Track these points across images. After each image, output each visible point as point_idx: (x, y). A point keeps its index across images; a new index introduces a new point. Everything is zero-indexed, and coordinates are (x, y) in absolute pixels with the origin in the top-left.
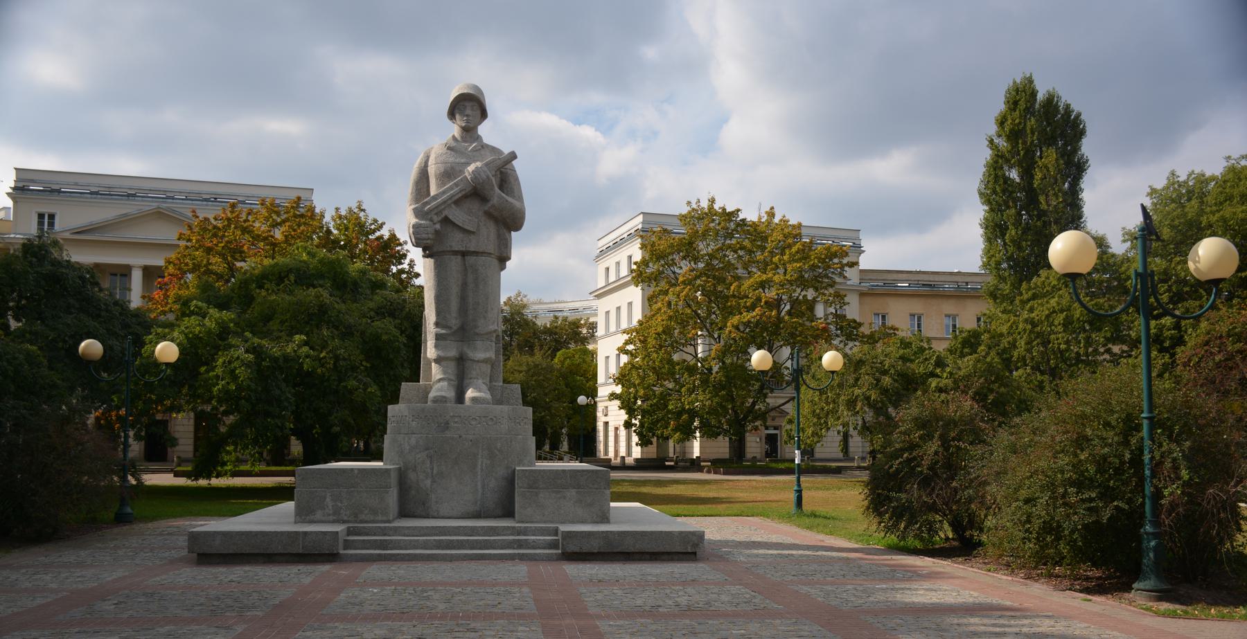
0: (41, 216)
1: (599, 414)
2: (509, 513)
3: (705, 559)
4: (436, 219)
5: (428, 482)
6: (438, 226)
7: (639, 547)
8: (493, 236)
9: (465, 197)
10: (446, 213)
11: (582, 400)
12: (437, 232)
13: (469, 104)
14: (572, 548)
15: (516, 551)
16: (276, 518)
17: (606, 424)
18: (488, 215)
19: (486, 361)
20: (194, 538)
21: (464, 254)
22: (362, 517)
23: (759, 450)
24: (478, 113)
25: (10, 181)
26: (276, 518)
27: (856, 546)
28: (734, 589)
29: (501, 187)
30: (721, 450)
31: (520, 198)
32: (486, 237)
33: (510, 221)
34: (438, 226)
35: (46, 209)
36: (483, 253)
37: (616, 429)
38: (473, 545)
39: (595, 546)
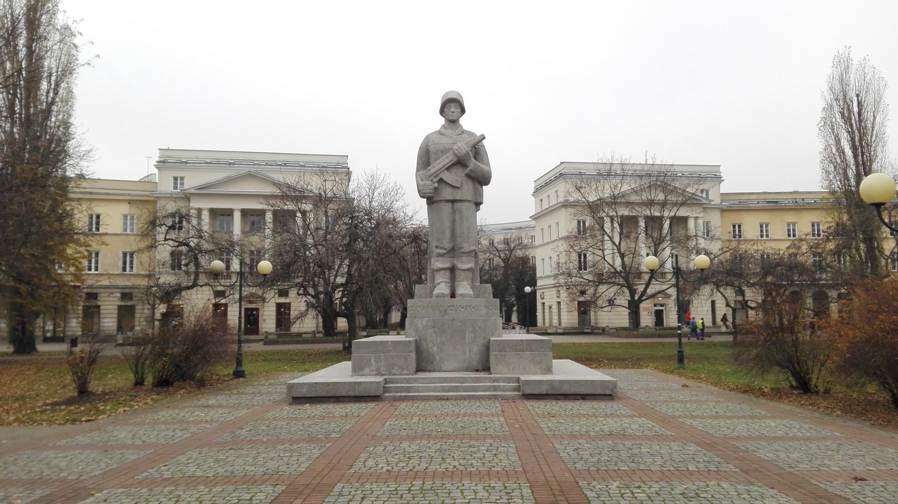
0: (175, 179)
1: (538, 297)
2: (487, 369)
3: (619, 398)
4: (435, 180)
5: (435, 349)
6: (436, 185)
7: (573, 390)
8: (471, 190)
9: (453, 165)
10: (441, 176)
11: (528, 289)
12: (436, 189)
13: (453, 105)
14: (528, 391)
15: (493, 393)
16: (338, 373)
17: (543, 304)
18: (468, 176)
19: (469, 270)
20: (291, 387)
21: (453, 202)
22: (394, 371)
23: (650, 321)
24: (459, 110)
25: (156, 158)
26: (338, 373)
27: (863, 254)
28: (641, 420)
29: (475, 158)
30: (623, 321)
31: (488, 164)
32: (467, 190)
33: (482, 179)
34: (436, 185)
35: (178, 174)
36: (465, 201)
37: (550, 307)
38: (466, 389)
39: (544, 390)
